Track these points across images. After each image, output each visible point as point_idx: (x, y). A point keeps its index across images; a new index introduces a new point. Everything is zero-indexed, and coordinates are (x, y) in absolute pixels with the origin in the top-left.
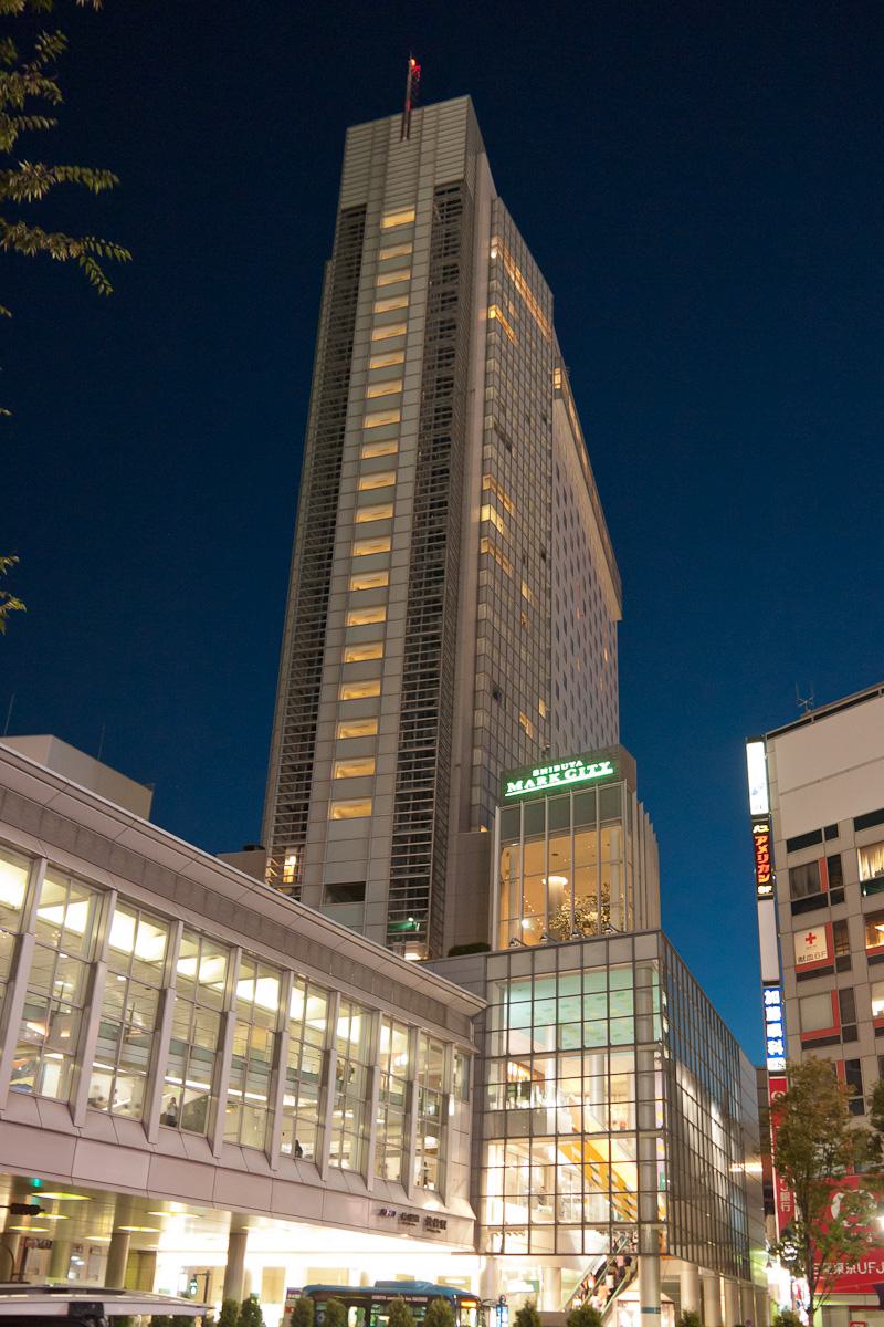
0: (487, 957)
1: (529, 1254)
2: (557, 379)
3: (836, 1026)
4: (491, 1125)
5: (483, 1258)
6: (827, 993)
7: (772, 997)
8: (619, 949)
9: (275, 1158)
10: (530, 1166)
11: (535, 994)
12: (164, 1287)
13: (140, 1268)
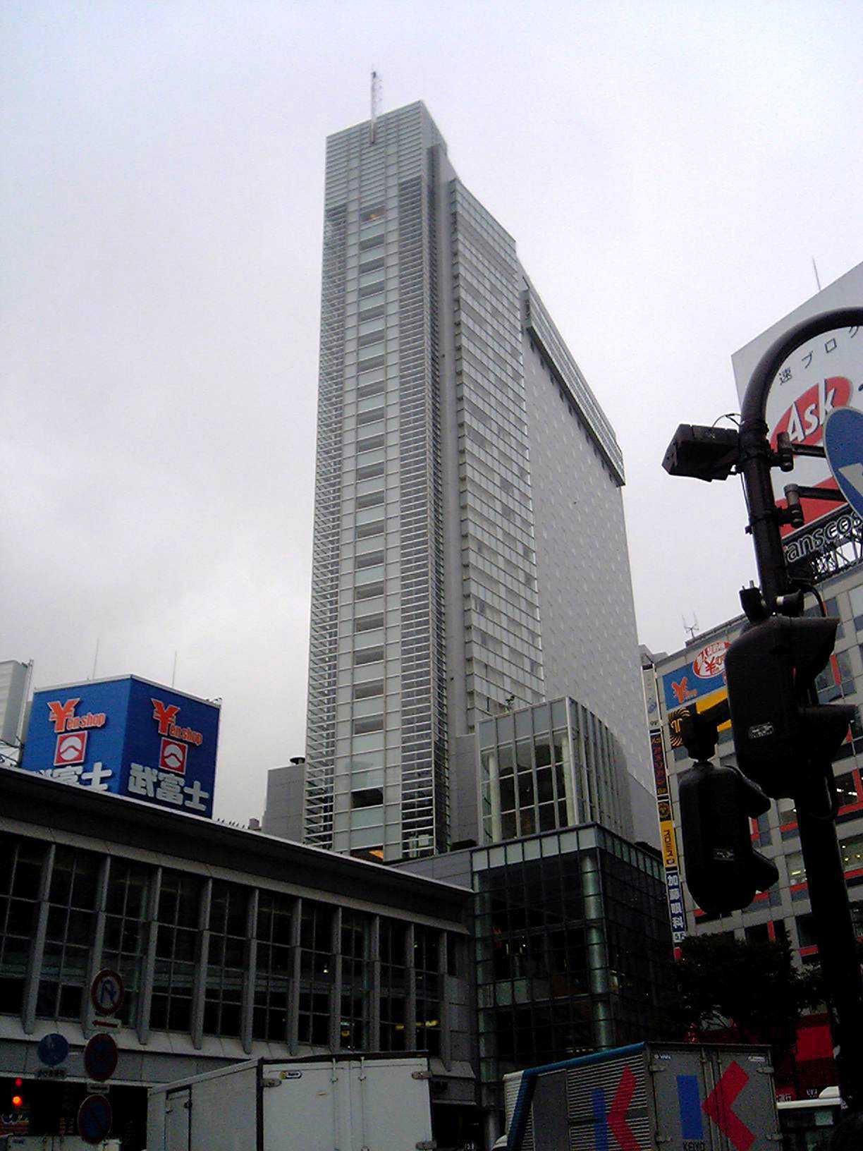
0: (472, 852)
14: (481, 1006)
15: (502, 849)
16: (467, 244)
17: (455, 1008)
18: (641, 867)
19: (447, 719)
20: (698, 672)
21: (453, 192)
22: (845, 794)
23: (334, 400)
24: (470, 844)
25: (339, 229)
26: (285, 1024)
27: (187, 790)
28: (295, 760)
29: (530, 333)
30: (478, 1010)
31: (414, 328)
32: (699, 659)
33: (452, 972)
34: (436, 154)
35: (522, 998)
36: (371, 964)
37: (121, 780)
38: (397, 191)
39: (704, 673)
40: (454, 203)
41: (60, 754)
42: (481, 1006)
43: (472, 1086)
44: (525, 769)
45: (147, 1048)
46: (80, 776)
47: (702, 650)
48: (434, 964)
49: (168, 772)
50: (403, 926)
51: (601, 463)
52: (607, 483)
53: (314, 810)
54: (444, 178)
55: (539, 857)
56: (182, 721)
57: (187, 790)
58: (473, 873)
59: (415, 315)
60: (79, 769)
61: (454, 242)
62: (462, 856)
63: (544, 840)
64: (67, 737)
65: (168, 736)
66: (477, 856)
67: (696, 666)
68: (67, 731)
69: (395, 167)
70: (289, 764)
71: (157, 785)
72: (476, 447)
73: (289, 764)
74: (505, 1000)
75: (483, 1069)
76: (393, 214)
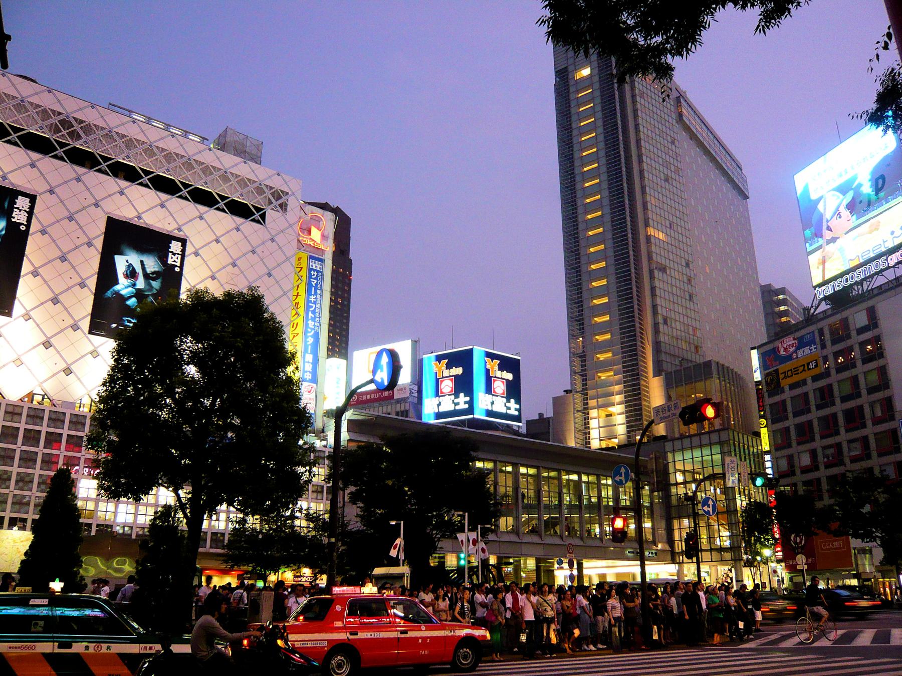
0: (665, 442)
1: (712, 561)
2: (217, 334)
3: (789, 470)
4: (674, 512)
5: (677, 565)
6: (806, 451)
7: (767, 457)
8: (715, 437)
9: (521, 534)
10: (680, 529)
11: (694, 454)
12: (653, 577)
13: (548, 577)
18: (478, 669)
20: (779, 352)
26: (32, 524)
27: (508, 404)
28: (567, 391)
31: (612, 127)
32: (780, 345)
37: (580, 477)
38: (600, 107)
39: (782, 353)
41: (441, 389)
45: (501, 540)
46: (453, 401)
47: (781, 340)
49: (497, 396)
56: (501, 368)
57: (508, 404)
59: (615, 158)
60: (453, 397)
64: (443, 380)
65: (495, 377)
67: (778, 349)
68: (443, 377)
70: (563, 394)
71: (493, 403)
73: (563, 394)
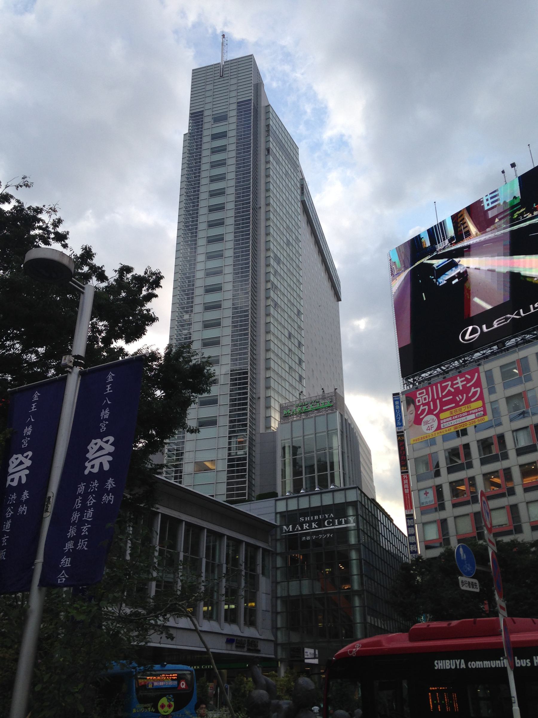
0: (276, 500)
14: (279, 595)
15: (307, 498)
16: (274, 144)
17: (264, 595)
19: (255, 422)
21: (268, 112)
22: (83, 588)
23: (190, 227)
24: (273, 495)
25: (197, 126)
29: (303, 203)
30: (277, 598)
33: (263, 574)
34: (258, 87)
35: (306, 591)
36: (220, 566)
40: (268, 119)
42: (279, 595)
43: (272, 645)
44: (309, 452)
48: (254, 570)
50: (239, 542)
51: (330, 286)
52: (332, 298)
53: (168, 472)
54: (263, 104)
55: (332, 503)
58: (276, 513)
61: (268, 142)
62: (270, 502)
63: (323, 495)
66: (279, 503)
69: (211, 104)
72: (275, 264)
74: (294, 592)
75: (279, 634)
76: (233, 120)
